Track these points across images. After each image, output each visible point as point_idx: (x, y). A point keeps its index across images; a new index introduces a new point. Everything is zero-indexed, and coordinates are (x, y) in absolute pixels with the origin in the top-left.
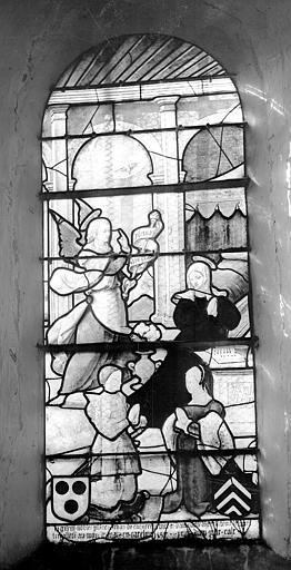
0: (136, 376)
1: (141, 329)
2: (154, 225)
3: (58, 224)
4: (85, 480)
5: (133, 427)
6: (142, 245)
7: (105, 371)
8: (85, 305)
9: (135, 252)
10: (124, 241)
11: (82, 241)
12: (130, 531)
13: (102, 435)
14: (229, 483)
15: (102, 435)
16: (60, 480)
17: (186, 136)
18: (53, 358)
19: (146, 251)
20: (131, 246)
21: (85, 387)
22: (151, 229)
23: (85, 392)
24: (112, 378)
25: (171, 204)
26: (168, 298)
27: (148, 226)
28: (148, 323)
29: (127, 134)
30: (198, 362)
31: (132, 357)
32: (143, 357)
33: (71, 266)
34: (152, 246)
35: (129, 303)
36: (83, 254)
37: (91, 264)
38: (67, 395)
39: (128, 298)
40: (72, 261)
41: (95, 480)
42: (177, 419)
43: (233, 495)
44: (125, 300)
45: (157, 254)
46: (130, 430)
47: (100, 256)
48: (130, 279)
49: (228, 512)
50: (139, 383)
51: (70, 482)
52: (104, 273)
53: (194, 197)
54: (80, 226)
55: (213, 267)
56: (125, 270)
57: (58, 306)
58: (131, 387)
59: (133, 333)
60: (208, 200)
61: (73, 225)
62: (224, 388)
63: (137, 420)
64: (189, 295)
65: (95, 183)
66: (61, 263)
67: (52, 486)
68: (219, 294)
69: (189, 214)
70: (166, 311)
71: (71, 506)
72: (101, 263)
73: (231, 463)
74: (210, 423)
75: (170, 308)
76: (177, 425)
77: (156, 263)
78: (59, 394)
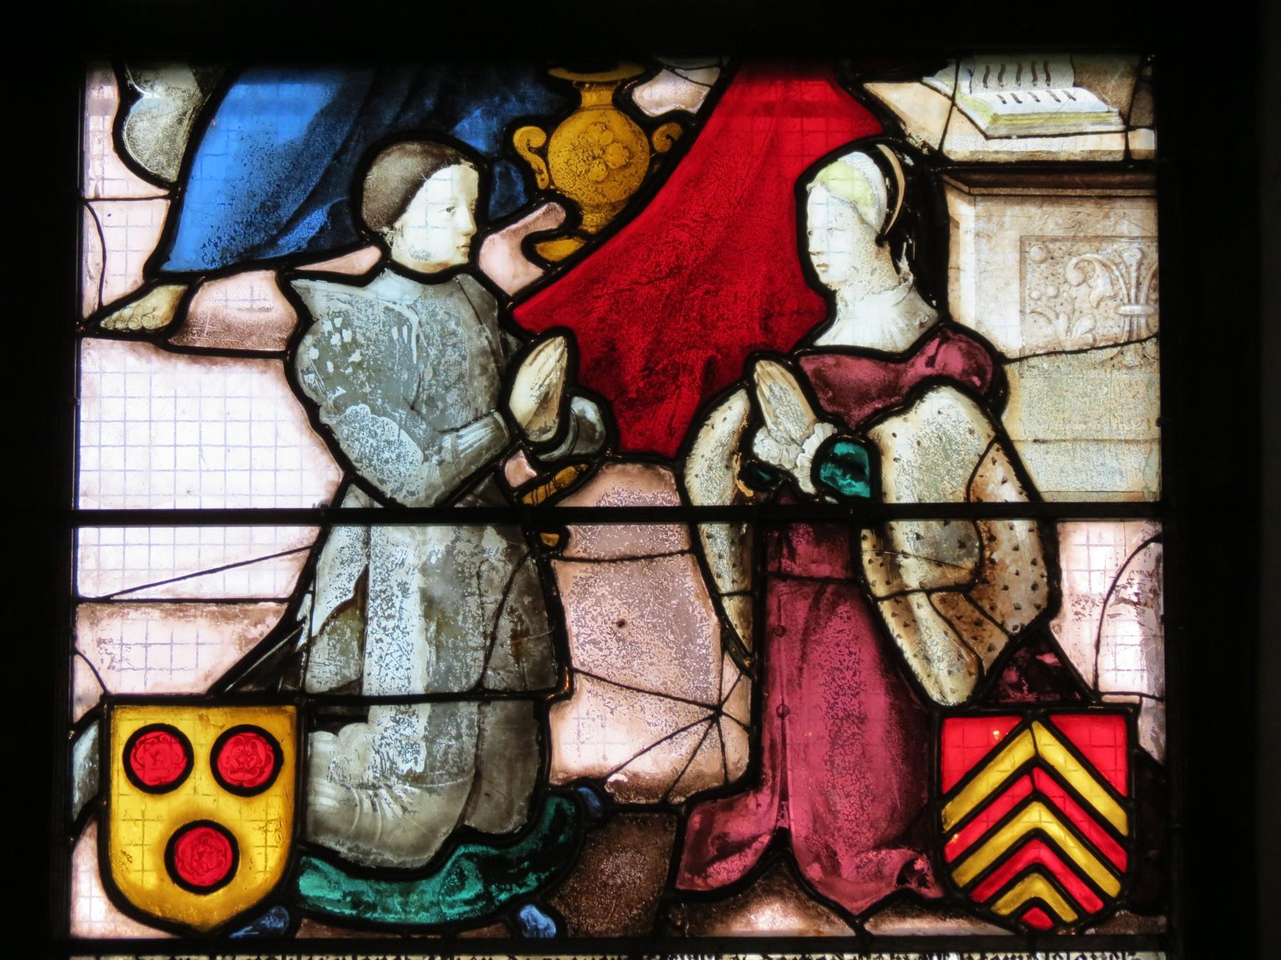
0: (552, 195)
4: (278, 724)
5: (535, 453)
7: (391, 170)
14: (1018, 754)
16: (118, 766)
18: (128, 98)
24: (436, 213)
31: (534, 96)
32: (589, 98)
38: (192, 282)
41: (334, 725)
42: (755, 420)
43: (1037, 816)
49: (1005, 906)
50: (571, 227)
51: (202, 731)
59: (361, 503)
62: (1000, 273)
63: (551, 419)
65: (110, 434)
73: (859, 929)
74: (925, 445)
76: (765, 448)
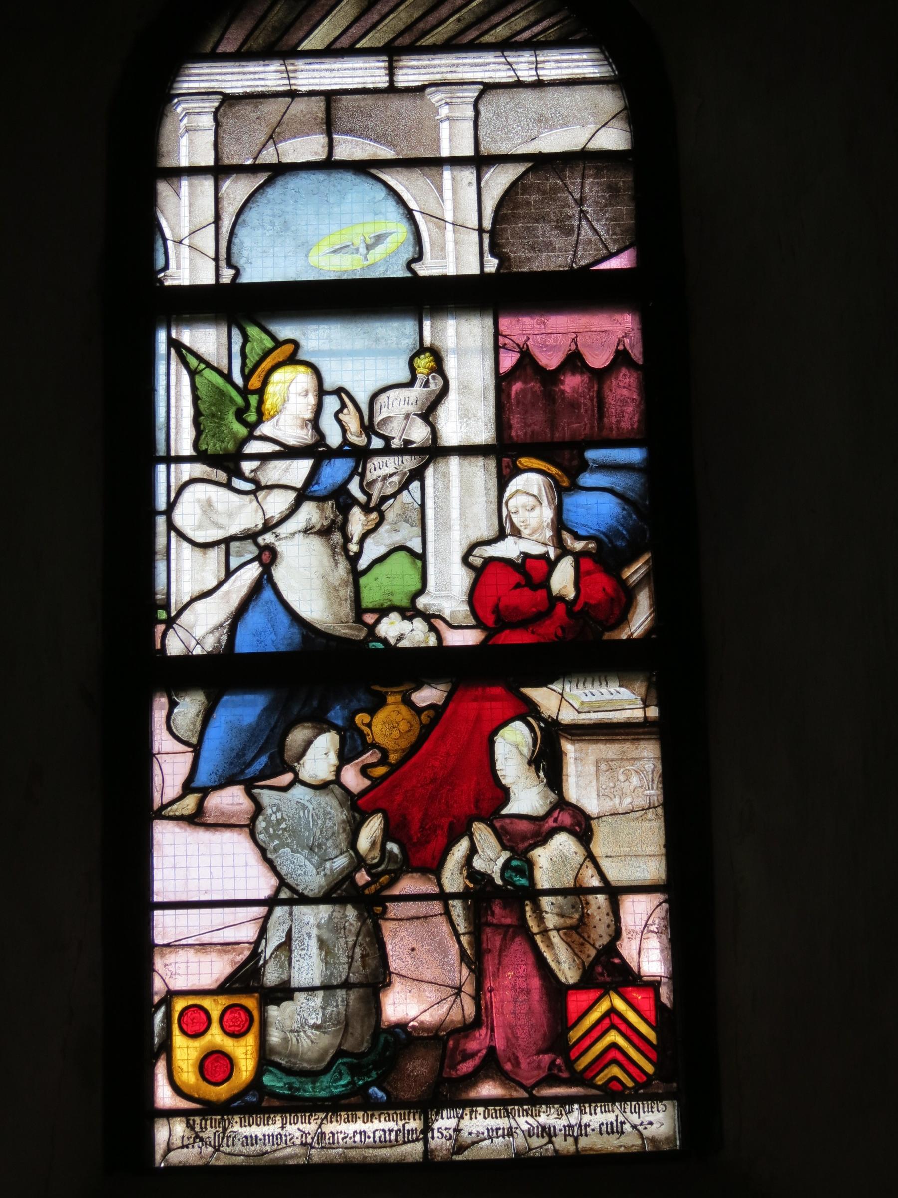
0: (374, 745)
1: (391, 628)
2: (426, 384)
3: (193, 374)
4: (251, 1003)
5: (369, 869)
6: (396, 432)
7: (298, 736)
8: (253, 571)
9: (377, 443)
10: (353, 424)
11: (252, 417)
12: (359, 1125)
13: (267, 918)
15: (267, 918)
17: (499, 180)
18: (173, 705)
19: (407, 442)
20: (368, 429)
21: (251, 772)
22: (417, 392)
23: (250, 787)
25: (465, 340)
26: (457, 557)
27: (410, 384)
28: (409, 612)
29: (363, 168)
30: (528, 711)
31: (364, 699)
32: (390, 699)
33: (222, 476)
34: (419, 433)
35: (363, 564)
36: (254, 447)
37: (276, 472)
38: (205, 792)
39: (359, 555)
40: (226, 463)
41: (278, 1002)
42: (473, 850)
44: (354, 559)
45: (434, 451)
46: (362, 877)
47: (289, 453)
48: (366, 509)
51: (214, 1007)
52: (303, 495)
53: (522, 327)
54: (247, 378)
55: (565, 483)
56: (354, 487)
57: (185, 573)
58: (364, 771)
60: (551, 335)
61: (228, 377)
62: (585, 777)
64: (509, 549)
66: (199, 469)
67: (168, 1016)
68: (579, 545)
69: (508, 361)
70: (449, 590)
71: (215, 1065)
72: (298, 471)
75: (459, 580)
77: (429, 473)
78: (188, 787)
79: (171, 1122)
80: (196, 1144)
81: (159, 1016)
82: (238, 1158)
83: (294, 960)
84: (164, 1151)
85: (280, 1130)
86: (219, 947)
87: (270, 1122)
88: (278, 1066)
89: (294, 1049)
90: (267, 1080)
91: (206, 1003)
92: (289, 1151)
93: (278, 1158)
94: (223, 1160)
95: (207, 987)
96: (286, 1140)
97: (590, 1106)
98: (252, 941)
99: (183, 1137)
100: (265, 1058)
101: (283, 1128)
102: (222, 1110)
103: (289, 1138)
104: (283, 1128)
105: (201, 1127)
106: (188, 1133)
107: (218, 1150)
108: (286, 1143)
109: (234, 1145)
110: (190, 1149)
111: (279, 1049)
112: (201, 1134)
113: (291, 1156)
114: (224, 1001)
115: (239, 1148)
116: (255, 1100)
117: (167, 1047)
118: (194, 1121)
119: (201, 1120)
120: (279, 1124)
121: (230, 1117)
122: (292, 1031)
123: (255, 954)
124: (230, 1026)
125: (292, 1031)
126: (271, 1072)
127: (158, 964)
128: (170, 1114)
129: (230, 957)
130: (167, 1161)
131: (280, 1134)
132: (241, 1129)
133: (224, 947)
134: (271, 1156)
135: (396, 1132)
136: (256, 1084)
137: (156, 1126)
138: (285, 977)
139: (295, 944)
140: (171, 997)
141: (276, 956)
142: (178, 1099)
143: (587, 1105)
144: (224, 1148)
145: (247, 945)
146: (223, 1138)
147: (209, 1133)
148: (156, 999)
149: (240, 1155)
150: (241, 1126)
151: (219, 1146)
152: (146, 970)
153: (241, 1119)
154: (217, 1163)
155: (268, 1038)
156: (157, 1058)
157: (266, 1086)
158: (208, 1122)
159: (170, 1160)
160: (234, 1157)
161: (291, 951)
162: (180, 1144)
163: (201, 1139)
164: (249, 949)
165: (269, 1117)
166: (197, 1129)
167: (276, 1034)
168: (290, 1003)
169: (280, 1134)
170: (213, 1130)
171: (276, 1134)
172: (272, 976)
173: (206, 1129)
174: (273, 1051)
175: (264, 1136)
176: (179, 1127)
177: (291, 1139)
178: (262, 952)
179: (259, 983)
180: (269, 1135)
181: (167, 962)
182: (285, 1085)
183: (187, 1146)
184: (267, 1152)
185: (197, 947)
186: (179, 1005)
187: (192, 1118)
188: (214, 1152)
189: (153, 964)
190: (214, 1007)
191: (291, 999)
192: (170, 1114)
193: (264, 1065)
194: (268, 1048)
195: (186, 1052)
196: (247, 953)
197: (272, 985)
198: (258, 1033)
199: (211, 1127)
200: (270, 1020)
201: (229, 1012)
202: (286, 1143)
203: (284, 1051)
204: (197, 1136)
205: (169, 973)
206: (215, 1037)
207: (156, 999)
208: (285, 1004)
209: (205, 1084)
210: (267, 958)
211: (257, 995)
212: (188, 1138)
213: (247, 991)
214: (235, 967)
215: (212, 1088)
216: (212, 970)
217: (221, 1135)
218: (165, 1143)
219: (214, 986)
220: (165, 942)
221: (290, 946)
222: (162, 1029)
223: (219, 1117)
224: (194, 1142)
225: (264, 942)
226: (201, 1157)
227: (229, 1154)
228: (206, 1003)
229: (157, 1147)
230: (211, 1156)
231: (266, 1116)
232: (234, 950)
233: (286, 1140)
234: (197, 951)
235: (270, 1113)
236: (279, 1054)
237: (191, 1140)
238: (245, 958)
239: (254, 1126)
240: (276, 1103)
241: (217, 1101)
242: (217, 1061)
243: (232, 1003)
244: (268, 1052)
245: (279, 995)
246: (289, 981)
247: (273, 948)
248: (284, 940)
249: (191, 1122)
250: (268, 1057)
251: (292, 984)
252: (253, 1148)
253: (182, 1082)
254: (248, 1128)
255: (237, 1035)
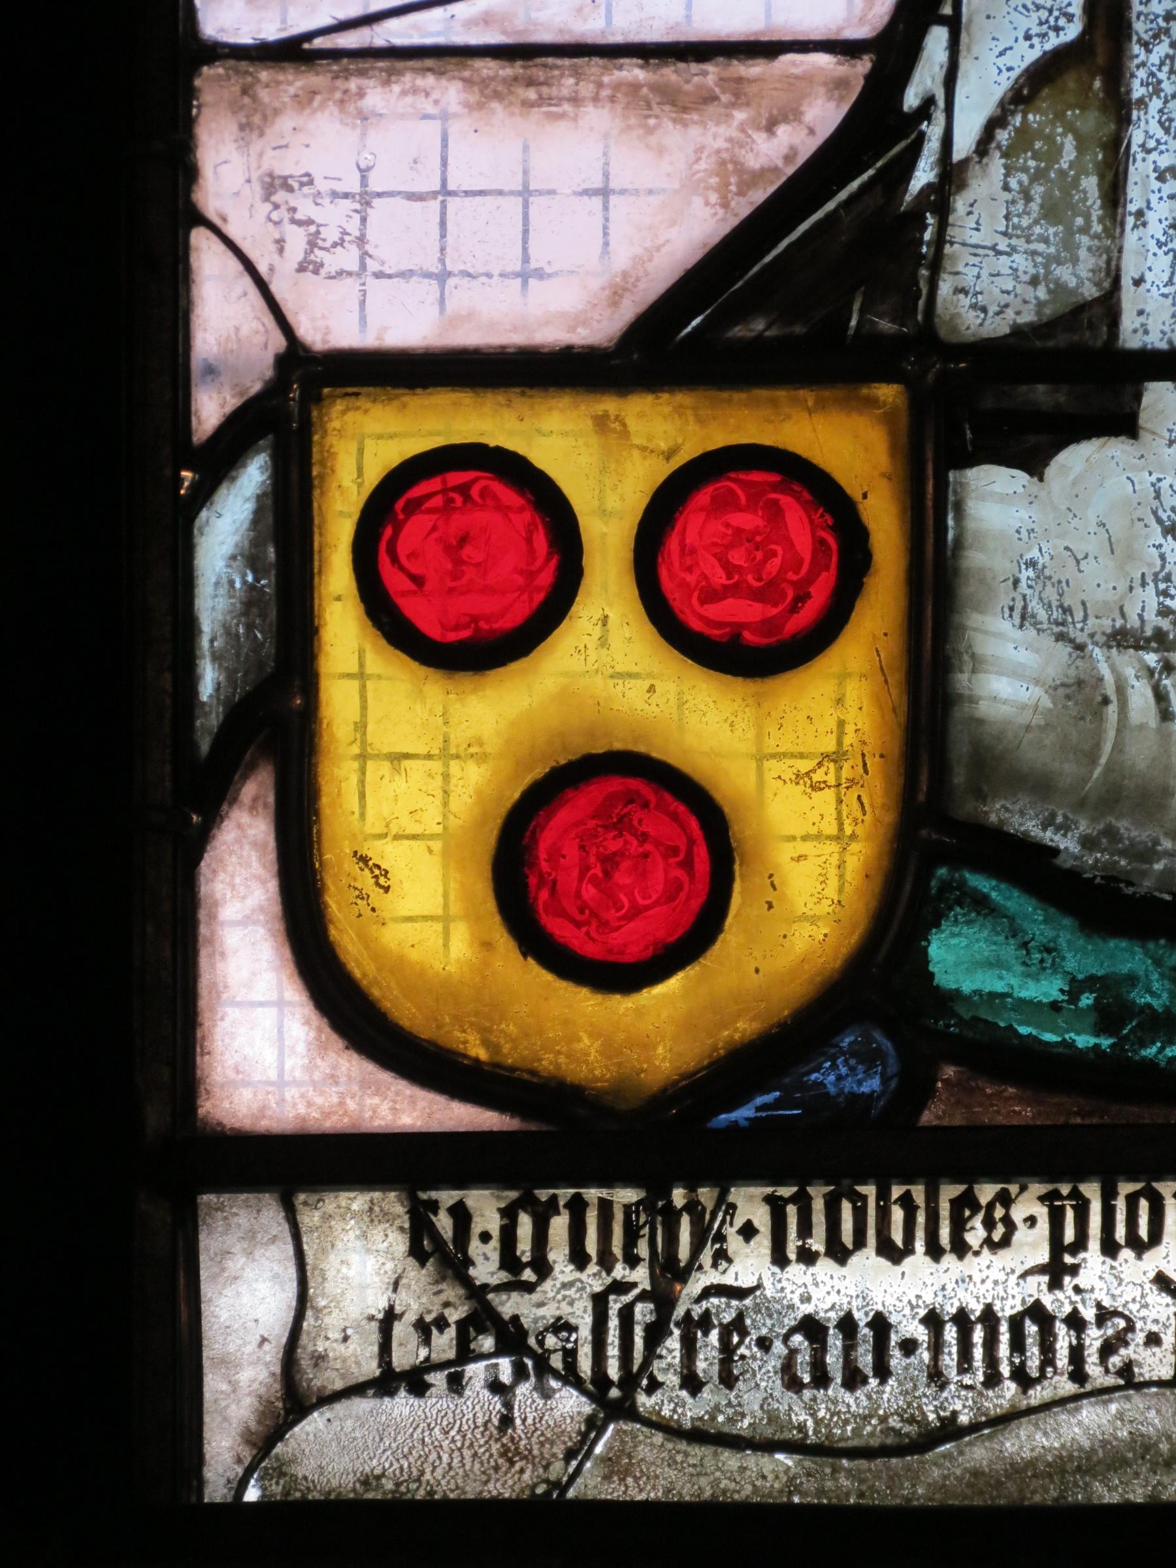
51: (604, 465)
71: (602, 851)
79: (309, 1219)
80: (476, 1371)
81: (226, 527)
82: (753, 1461)
83: (1140, 171)
84: (265, 1410)
85: (1036, 1288)
86: (633, 72)
87: (975, 1235)
88: (1029, 865)
89: (1140, 755)
90: (959, 958)
91: (554, 438)
92: (1091, 1423)
93: (1020, 1470)
94: (661, 1474)
95: (551, 335)
96: (1077, 1354)
97: (1108, 1196)
98: (862, 32)
99: (390, 1317)
100: (944, 817)
101: (1056, 1271)
102: (662, 1148)
103: (1094, 1338)
104: (1056, 1271)
105: (509, 1261)
106: (419, 1295)
107: (625, 1410)
108: (1078, 1374)
109: (728, 1380)
110: (438, 1401)
111: (1037, 754)
112: (509, 1305)
113: (1108, 1459)
114: (663, 430)
115: (760, 1395)
116: (872, 1085)
117: (280, 726)
118: (461, 1215)
119: (509, 1214)
120: (1033, 1246)
121: (706, 1195)
122: (1123, 639)
123: (880, 124)
124: (711, 595)
125: (1123, 639)
126: (981, 905)
127: (226, 171)
128: (299, 1166)
129: (713, 135)
130: (280, 1471)
131: (1036, 1311)
132: (779, 1275)
133: (670, 73)
134: (978, 1454)
135: (726, 1332)
136: (879, 978)
137: (209, 1243)
138: (1080, 277)
139: (1146, 63)
140: (312, 397)
141: (1024, 138)
142: (353, 1066)
143: (1092, 1191)
144: (667, 1401)
145: (823, 60)
146: (656, 1334)
147: (563, 1296)
148: (210, 409)
149: (769, 1446)
150: (780, 1259)
151: (629, 1381)
152: (147, 219)
153: (776, 1206)
154: (613, 1491)
155: (962, 680)
156: (210, 798)
157: (948, 999)
158: (559, 1225)
159: (305, 1469)
160: (731, 1460)
161: (1120, 109)
162: (371, 1368)
163: (512, 1338)
164: (841, 84)
165: (965, 1204)
166: (486, 1267)
167: (1024, 656)
168: (1116, 449)
169: (1036, 1311)
170: (594, 1280)
171: (1007, 1309)
172: (993, 270)
173: (543, 1268)
174: (995, 766)
175: (933, 1320)
176: (363, 1260)
177: (1107, 1349)
178: (925, 109)
179: (904, 312)
180: (962, 1319)
181: (288, 165)
182: (1075, 989)
183: (415, 1381)
184: (949, 1429)
185: (487, 67)
186: (365, 445)
187: (447, 1197)
188: (594, 1426)
189: (191, 173)
190: (604, 465)
191: (1124, 424)
192: (299, 1166)
193: (935, 856)
194: (960, 748)
195: (414, 769)
196: (824, 116)
197: (997, 327)
198: (893, 647)
199: (579, 1258)
200: (974, 558)
201: (703, 497)
202: (1078, 1374)
203: (1069, 769)
204: (482, 1316)
205: (297, 240)
206: (607, 667)
207: (210, 409)
208: (1076, 460)
209: (538, 975)
210: (963, 145)
211: (888, 393)
212: (424, 1329)
213: (823, 363)
214: (743, 208)
215: (585, 1004)
216: (590, 219)
217: (643, 1313)
218: (272, 1355)
219: (600, 328)
220: (271, 32)
221: (1116, 75)
222: (252, 602)
223: (627, 1195)
224: (465, 1354)
225: (937, 40)
226: (510, 1455)
227: (698, 1435)
228: (554, 438)
229: (213, 1384)
230: (578, 1450)
231: (949, 1192)
232: (738, 90)
233: (1077, 1354)
234: (488, 94)
235: (970, 1175)
236: (1040, 786)
237: (444, 1344)
238: (808, 146)
239: (867, 1260)
240: (1012, 1108)
241: (620, 1088)
242: (621, 825)
243: (719, 439)
244: (959, 777)
245: (1041, 394)
246: (1108, 305)
247: (1002, 85)
248: (1072, 31)
249: (444, 1223)
250: (966, 808)
251: (1128, 322)
252: (853, 1402)
253: (378, 954)
254: (825, 1267)
255: (750, 656)
